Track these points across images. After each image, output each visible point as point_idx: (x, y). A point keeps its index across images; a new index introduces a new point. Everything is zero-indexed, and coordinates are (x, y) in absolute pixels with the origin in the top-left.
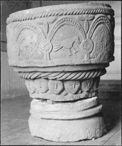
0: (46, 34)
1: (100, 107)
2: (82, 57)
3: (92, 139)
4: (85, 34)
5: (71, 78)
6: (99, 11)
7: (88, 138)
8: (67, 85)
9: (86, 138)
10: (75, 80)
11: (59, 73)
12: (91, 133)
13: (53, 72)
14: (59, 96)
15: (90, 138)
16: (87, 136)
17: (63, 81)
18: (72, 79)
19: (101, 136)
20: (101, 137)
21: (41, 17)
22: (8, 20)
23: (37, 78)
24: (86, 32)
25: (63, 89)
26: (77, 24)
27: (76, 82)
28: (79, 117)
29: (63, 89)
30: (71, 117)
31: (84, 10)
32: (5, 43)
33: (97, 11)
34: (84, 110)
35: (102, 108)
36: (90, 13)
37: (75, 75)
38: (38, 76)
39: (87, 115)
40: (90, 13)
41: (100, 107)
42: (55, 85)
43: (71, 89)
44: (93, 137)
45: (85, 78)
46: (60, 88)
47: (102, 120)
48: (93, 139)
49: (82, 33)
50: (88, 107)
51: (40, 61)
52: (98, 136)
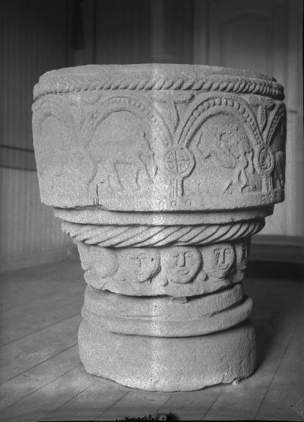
0: (172, 131)
1: (248, 305)
3: (231, 383)
5: (116, 245)
6: (252, 87)
7: (224, 382)
10: (227, 242)
11: (190, 228)
17: (199, 246)
18: (156, 245)
19: (251, 373)
20: (251, 375)
21: (109, 88)
22: (37, 89)
23: (138, 245)
26: (246, 114)
28: (205, 330)
30: (200, 331)
32: (29, 154)
33: (247, 87)
35: (254, 306)
36: (242, 90)
37: (228, 231)
39: (223, 327)
41: (248, 305)
42: (181, 257)
43: (173, 267)
45: (246, 234)
48: (234, 383)
50: (224, 307)
51: (259, 193)
52: (245, 374)
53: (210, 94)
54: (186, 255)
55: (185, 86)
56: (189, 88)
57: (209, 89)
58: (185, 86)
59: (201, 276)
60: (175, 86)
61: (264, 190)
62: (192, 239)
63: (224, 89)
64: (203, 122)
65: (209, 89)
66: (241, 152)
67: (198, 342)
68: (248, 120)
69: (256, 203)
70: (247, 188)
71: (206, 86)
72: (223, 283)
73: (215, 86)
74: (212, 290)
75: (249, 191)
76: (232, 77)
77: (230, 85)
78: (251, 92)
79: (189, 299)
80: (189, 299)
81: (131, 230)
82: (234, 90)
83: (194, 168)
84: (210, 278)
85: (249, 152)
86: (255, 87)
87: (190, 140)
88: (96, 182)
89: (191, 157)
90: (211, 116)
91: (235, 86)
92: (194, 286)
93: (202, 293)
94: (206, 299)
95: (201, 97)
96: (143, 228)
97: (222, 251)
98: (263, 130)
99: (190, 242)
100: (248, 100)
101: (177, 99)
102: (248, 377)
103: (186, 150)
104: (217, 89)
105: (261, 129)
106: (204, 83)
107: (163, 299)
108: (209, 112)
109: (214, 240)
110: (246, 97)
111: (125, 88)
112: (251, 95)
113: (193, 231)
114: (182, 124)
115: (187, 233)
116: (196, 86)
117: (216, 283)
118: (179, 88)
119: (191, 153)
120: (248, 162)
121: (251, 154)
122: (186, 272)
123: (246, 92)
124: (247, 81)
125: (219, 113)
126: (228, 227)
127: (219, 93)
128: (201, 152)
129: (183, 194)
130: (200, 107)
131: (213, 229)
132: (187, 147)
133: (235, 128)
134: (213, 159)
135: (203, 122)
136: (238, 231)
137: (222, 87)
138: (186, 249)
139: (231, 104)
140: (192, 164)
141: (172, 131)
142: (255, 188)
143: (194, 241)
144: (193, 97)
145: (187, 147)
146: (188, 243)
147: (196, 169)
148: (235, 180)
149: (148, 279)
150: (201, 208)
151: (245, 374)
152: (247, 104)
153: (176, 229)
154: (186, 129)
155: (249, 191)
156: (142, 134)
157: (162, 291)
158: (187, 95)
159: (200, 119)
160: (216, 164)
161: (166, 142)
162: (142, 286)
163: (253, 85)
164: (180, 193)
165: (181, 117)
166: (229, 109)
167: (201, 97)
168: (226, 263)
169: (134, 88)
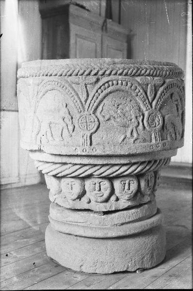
0: (84, 103)
2: (118, 139)
4: (82, 106)
8: (117, 184)
9: (125, 270)
12: (133, 261)
13: (103, 165)
14: (102, 205)
15: (133, 270)
16: (126, 266)
17: (111, 179)
20: (153, 268)
23: (68, 176)
24: (83, 100)
25: (84, 193)
26: (137, 90)
27: (131, 179)
28: (114, 234)
29: (84, 193)
31: (171, 71)
33: (139, 72)
34: (122, 224)
36: (156, 74)
38: (58, 174)
40: (156, 74)
42: (97, 185)
44: (138, 269)
46: (77, 189)
47: (157, 241)
48: (137, 271)
49: (75, 101)
53: (109, 78)
54: (101, 183)
55: (93, 73)
56: (95, 75)
57: (110, 74)
58: (93, 73)
59: (113, 198)
60: (86, 73)
61: (154, 141)
62: (103, 173)
63: (121, 74)
64: (104, 97)
65: (110, 74)
66: (133, 116)
67: (110, 242)
68: (139, 94)
69: (148, 150)
70: (138, 141)
71: (107, 72)
72: (129, 204)
73: (113, 72)
74: (121, 208)
75: (140, 142)
76: (126, 66)
77: (125, 71)
78: (142, 75)
79: (105, 213)
80: (105, 213)
81: (45, 165)
82: (128, 74)
83: (98, 127)
84: (92, 202)
85: (140, 116)
86: (146, 71)
87: (96, 109)
88: (40, 135)
89: (96, 120)
90: (110, 93)
91: (129, 72)
92: (108, 205)
93: (113, 209)
94: (117, 214)
95: (104, 80)
96: (70, 165)
97: (127, 182)
98: (153, 100)
99: (101, 176)
100: (139, 81)
101: (87, 82)
102: (150, 269)
103: (93, 115)
104: (116, 74)
105: (150, 100)
106: (105, 71)
107: (86, 212)
108: (109, 90)
109: (119, 174)
110: (138, 79)
111: (51, 75)
112: (143, 77)
113: (111, 169)
114: (90, 99)
115: (99, 169)
116: (100, 73)
117: (124, 203)
118: (89, 74)
119: (96, 117)
120: (139, 123)
121: (142, 117)
122: (101, 195)
123: (139, 75)
124: (139, 67)
125: (117, 90)
126: (128, 167)
127: (117, 77)
128: (104, 117)
129: (91, 144)
130: (103, 87)
131: (117, 168)
132: (94, 113)
133: (128, 100)
134: (112, 121)
135: (104, 97)
136: (117, 171)
137: (119, 72)
138: (100, 180)
139: (126, 84)
140: (97, 123)
141: (84, 103)
142: (145, 140)
143: (103, 175)
144: (98, 80)
145: (94, 113)
146: (99, 176)
147: (100, 128)
148: (128, 134)
149: (77, 198)
150: (103, 154)
151: (147, 266)
152: (139, 83)
153: (90, 166)
154: (93, 101)
155: (140, 142)
156: (65, 105)
157: (87, 206)
158: (94, 79)
159: (102, 95)
160: (115, 124)
161: (80, 111)
162: (74, 202)
163: (145, 70)
164: (89, 143)
165: (89, 92)
166: (123, 87)
167: (104, 80)
168: (131, 190)
169: (47, 75)
